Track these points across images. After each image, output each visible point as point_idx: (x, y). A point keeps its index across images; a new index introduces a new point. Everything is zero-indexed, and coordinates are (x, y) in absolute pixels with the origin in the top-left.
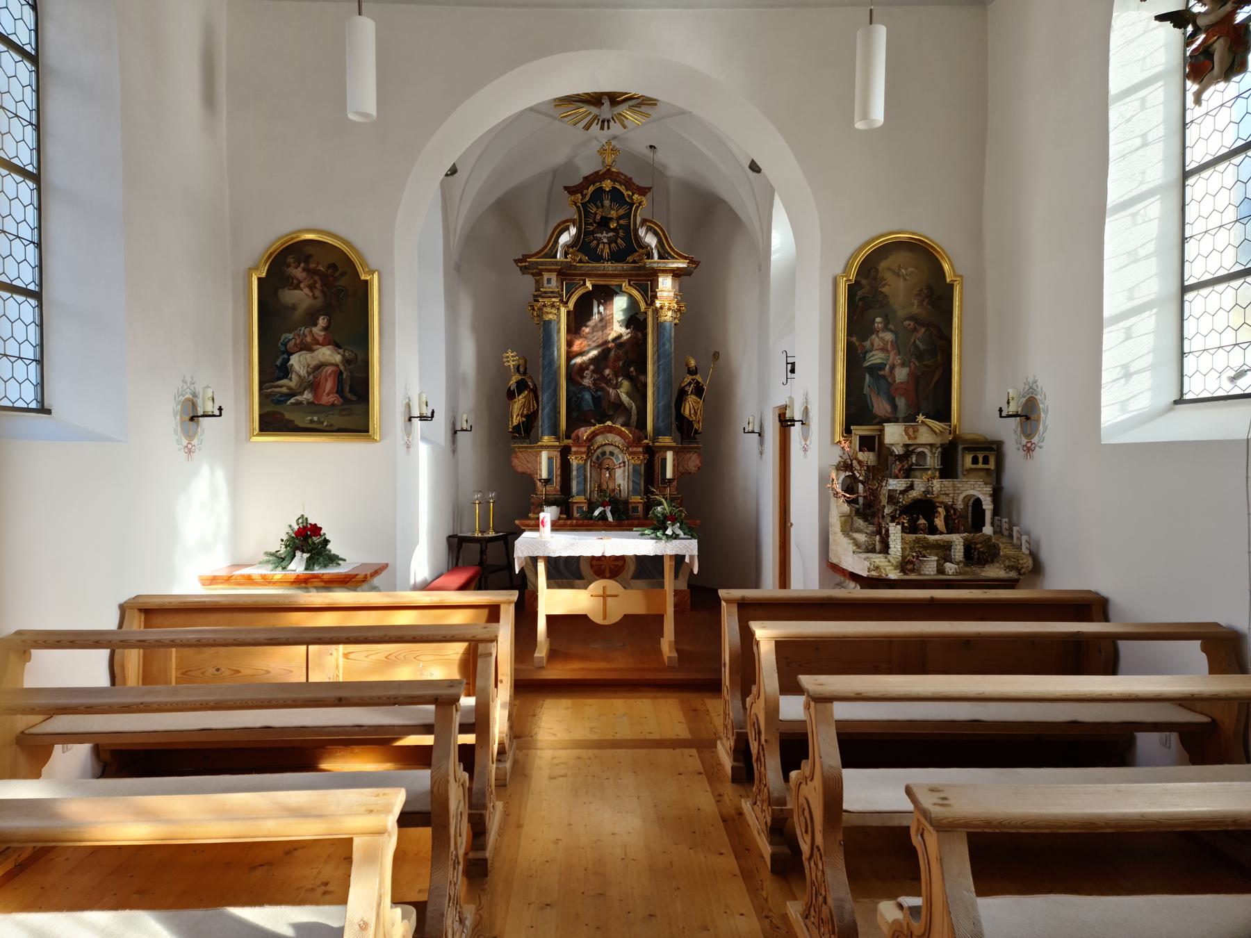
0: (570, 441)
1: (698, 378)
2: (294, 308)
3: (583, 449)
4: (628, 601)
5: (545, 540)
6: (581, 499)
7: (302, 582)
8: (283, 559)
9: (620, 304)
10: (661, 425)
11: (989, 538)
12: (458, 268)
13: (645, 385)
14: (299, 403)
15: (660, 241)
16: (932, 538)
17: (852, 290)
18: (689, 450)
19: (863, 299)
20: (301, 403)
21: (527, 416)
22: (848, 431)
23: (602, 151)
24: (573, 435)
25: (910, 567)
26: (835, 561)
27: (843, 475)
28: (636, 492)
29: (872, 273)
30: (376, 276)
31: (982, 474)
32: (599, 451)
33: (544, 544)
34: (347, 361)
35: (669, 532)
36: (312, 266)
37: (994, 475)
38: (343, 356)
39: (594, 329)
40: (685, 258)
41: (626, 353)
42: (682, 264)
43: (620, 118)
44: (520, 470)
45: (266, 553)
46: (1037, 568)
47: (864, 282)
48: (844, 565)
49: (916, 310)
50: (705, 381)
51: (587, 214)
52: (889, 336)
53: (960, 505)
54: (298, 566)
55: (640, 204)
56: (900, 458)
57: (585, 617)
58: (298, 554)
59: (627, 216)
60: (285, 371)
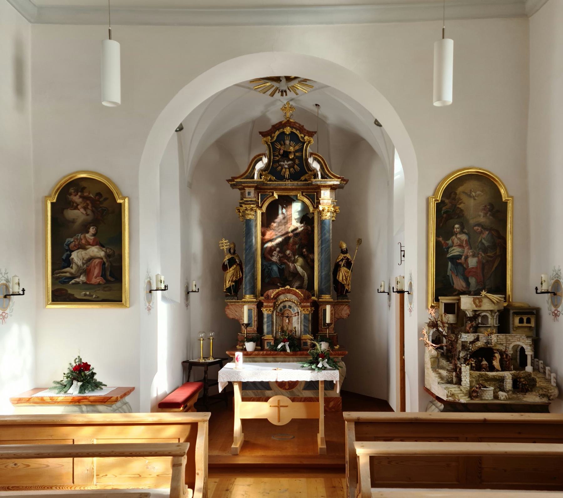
0: (263, 298)
1: (348, 256)
2: (73, 221)
3: (271, 304)
4: (297, 411)
5: (241, 370)
6: (270, 337)
7: (76, 402)
8: (65, 386)
9: (296, 207)
10: (323, 287)
11: (530, 374)
12: (190, 185)
13: (313, 261)
14: (78, 283)
15: (322, 167)
16: (491, 374)
17: (439, 206)
18: (342, 303)
19: (447, 213)
20: (78, 283)
21: (235, 282)
22: (437, 300)
23: (284, 108)
24: (265, 294)
25: (474, 394)
26: (428, 387)
27: (432, 331)
28: (306, 332)
29: (453, 196)
30: (127, 200)
31: (526, 329)
32: (282, 305)
33: (237, 373)
34: (108, 256)
35: (320, 365)
36: (86, 194)
37: (535, 331)
38: (106, 252)
39: (280, 224)
40: (339, 178)
41: (301, 239)
42: (336, 182)
43: (294, 89)
44: (231, 317)
45: (55, 382)
47: (447, 201)
48: (433, 391)
49: (482, 219)
50: (352, 257)
51: (275, 149)
52: (464, 237)
53: (510, 352)
54: (74, 391)
55: (309, 142)
57: (266, 420)
58: (75, 382)
59: (301, 150)
60: (68, 262)
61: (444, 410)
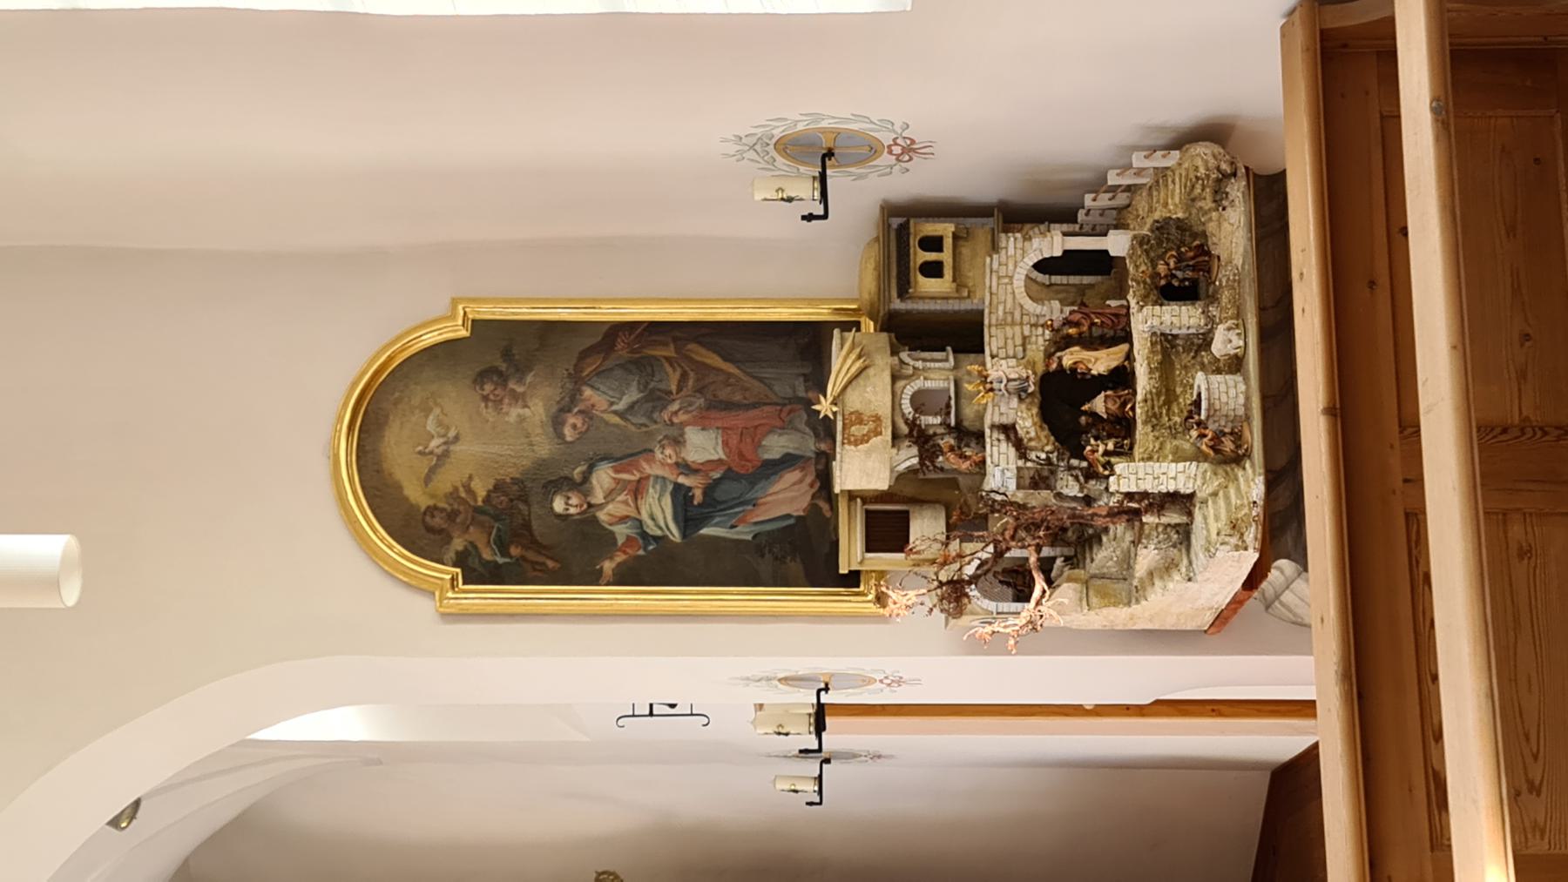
61: (1300, 556)
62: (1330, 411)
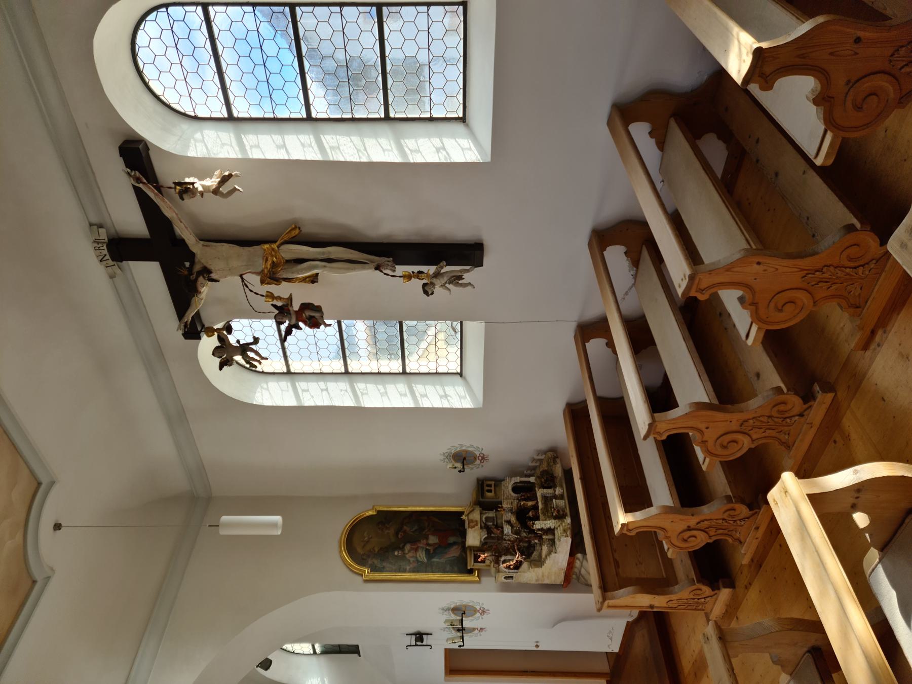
16: (540, 505)
22: (471, 572)
46: (554, 454)
48: (564, 564)
56: (489, 532)
61: (584, 552)
62: (581, 478)
